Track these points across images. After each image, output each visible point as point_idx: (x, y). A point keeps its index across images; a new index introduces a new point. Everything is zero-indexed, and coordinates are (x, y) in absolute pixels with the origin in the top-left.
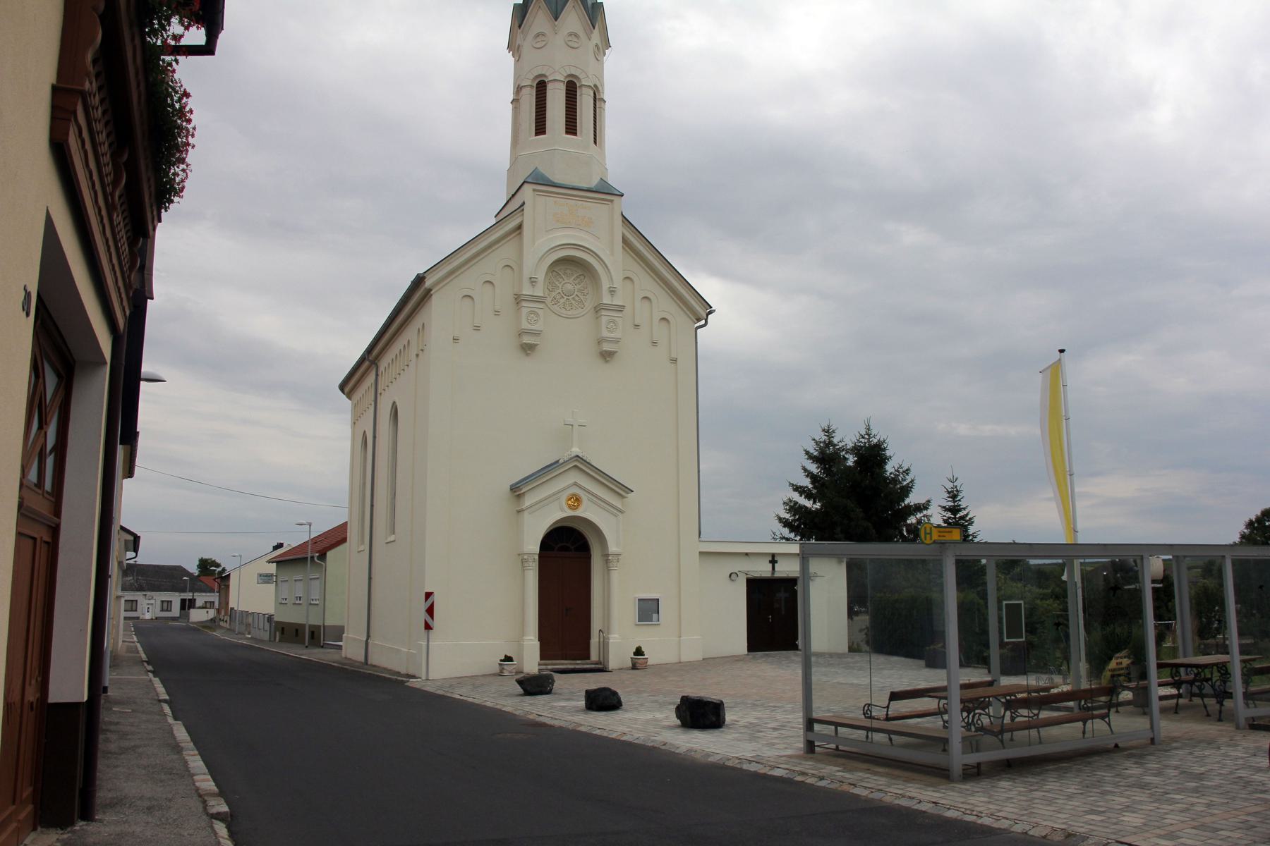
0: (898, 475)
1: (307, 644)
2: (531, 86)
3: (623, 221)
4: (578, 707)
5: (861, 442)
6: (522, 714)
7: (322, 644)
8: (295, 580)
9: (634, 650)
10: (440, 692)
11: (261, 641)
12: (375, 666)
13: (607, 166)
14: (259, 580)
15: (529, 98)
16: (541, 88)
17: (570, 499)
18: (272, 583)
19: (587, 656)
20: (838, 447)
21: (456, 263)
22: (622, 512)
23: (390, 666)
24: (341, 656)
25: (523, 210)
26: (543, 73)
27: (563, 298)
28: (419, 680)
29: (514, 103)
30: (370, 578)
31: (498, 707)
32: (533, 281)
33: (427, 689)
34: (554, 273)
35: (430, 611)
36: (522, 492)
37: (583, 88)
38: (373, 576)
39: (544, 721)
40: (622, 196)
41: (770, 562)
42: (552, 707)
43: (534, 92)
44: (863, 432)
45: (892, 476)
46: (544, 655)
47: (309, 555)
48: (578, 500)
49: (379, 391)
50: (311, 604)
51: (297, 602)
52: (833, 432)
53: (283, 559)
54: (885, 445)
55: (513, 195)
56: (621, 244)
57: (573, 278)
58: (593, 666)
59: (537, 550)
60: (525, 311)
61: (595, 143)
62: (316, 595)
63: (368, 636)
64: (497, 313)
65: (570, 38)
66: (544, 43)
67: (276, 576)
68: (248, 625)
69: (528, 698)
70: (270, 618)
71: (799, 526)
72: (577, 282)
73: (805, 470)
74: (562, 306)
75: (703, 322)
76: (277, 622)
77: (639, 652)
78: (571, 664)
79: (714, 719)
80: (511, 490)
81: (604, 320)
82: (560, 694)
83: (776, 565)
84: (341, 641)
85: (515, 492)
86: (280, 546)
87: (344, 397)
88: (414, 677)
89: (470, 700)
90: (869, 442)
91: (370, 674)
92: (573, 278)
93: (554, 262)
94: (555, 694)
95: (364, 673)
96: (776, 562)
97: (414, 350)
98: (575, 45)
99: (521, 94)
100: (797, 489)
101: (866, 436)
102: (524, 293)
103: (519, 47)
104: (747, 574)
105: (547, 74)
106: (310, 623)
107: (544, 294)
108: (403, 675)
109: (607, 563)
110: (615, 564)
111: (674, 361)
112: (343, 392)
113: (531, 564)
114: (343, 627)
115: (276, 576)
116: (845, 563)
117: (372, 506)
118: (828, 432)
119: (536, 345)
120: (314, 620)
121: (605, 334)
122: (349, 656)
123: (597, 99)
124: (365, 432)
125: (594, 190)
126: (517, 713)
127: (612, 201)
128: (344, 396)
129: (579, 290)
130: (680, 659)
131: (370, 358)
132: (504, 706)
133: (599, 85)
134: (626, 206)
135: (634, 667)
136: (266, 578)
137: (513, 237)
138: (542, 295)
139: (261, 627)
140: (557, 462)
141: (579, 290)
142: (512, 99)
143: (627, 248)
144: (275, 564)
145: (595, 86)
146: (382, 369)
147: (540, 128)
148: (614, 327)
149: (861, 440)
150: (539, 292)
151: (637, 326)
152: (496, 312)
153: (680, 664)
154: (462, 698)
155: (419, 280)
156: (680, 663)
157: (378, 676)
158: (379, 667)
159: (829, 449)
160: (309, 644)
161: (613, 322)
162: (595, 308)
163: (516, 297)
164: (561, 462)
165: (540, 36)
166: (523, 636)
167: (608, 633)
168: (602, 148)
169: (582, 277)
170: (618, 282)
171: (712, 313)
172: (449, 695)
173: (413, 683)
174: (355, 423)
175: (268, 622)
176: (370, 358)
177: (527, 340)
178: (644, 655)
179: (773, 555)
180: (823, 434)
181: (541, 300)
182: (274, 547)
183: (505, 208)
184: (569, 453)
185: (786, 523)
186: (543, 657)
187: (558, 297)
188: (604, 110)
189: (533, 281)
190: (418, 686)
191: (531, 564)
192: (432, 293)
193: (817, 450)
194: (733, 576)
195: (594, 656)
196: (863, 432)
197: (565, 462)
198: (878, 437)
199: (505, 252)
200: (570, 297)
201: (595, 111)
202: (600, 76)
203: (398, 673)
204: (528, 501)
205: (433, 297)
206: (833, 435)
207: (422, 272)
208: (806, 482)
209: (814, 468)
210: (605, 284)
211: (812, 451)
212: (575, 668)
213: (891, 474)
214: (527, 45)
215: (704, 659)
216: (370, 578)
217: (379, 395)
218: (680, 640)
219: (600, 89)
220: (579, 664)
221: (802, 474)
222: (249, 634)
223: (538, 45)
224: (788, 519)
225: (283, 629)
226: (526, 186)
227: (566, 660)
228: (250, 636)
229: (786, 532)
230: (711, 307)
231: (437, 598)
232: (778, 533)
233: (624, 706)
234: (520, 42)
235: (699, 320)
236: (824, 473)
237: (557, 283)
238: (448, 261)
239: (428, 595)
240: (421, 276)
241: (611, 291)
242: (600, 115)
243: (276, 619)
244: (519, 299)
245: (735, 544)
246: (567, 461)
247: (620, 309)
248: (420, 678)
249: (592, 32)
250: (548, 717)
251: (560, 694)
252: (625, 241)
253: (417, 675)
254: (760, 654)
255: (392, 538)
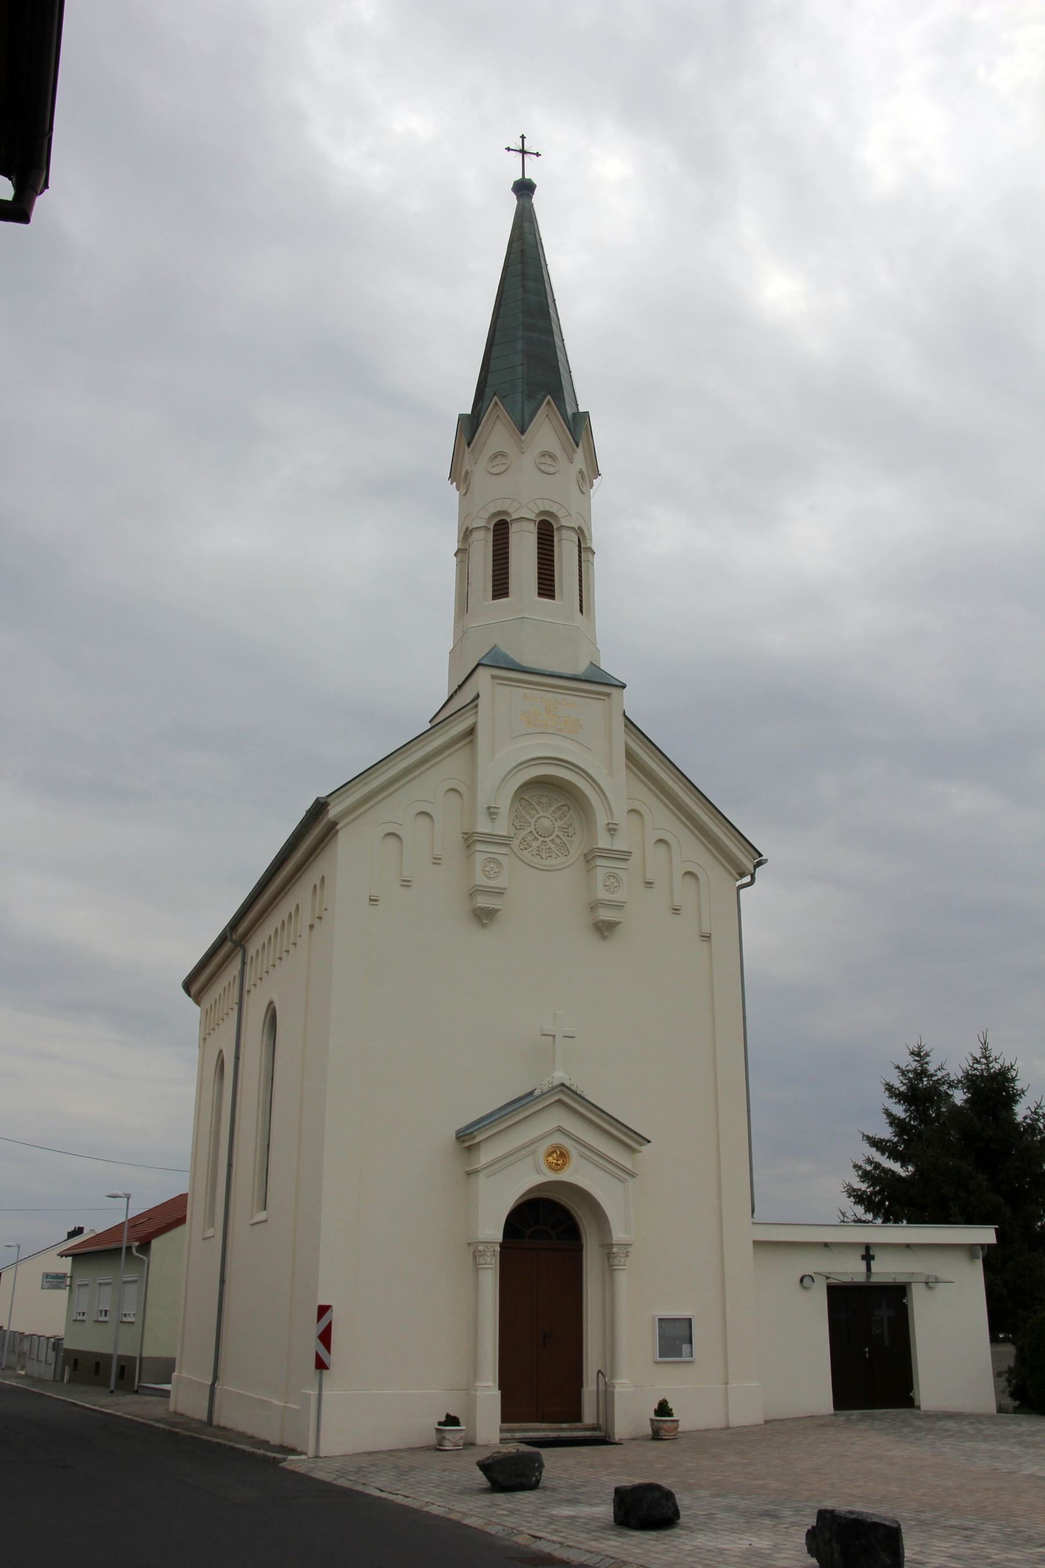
0: (1038, 1120)
1: (112, 1387)
2: (486, 528)
3: (626, 725)
4: (595, 1519)
5: (976, 1069)
6: (499, 1534)
7: (136, 1388)
8: (100, 1284)
9: (656, 1407)
10: (342, 1482)
11: (40, 1381)
12: (224, 1429)
13: (598, 646)
14: (45, 1283)
15: (483, 547)
16: (501, 531)
17: (550, 1154)
18: (65, 1289)
19: (576, 1416)
20: (935, 1078)
21: (374, 784)
22: (633, 1175)
23: (250, 1430)
24: (168, 1409)
25: (477, 706)
26: (504, 508)
27: (538, 839)
28: (303, 1457)
29: (459, 555)
30: (222, 1282)
31: (452, 1516)
32: (492, 813)
33: (318, 1475)
34: (523, 801)
35: (325, 1337)
36: (476, 1140)
37: (564, 531)
38: (227, 1278)
39: (547, 1550)
40: (624, 687)
41: (863, 1258)
42: (552, 1519)
43: (490, 536)
44: (978, 1055)
45: (1028, 1121)
46: (509, 1413)
47: (124, 1246)
48: (563, 1155)
49: (246, 988)
50: (122, 1322)
51: (100, 1319)
52: (927, 1055)
53: (90, 1249)
54: (1014, 1073)
55: (460, 687)
56: (624, 760)
57: (552, 809)
58: (588, 1434)
59: (498, 1235)
60: (479, 858)
61: (581, 611)
62: (131, 1310)
63: (215, 1378)
64: (437, 861)
65: (543, 460)
66: (504, 467)
67: (71, 1277)
68: (22, 1355)
69: (500, 1497)
70: (57, 1344)
71: (881, 1203)
72: (557, 815)
73: (889, 1114)
74: (535, 852)
75: (747, 879)
76: (67, 1351)
77: (663, 1409)
78: (551, 1430)
79: (888, 1561)
80: (458, 1138)
81: (600, 873)
82: (553, 1489)
83: (872, 1262)
84: (170, 1383)
85: (464, 1141)
86: (79, 1231)
87: (190, 1000)
88: (293, 1451)
89: (399, 1499)
90: (988, 1069)
91: (218, 1444)
92: (552, 809)
93: (519, 788)
94: (545, 1488)
95: (208, 1442)
96: (873, 1258)
97: (306, 918)
98: (551, 470)
99: (471, 540)
100: (877, 1144)
101: (983, 1060)
102: (479, 830)
103: (467, 473)
104: (827, 1278)
105: (510, 511)
106: (121, 1352)
107: (508, 832)
108: (273, 1446)
109: (609, 1258)
110: (622, 1260)
111: (706, 937)
112: (189, 994)
113: (489, 1259)
114: (174, 1359)
115: (71, 1277)
116: (981, 1258)
117: (230, 1165)
118: (918, 1054)
119: (497, 911)
120: (127, 1349)
121: (602, 894)
122: (180, 1410)
123: (584, 549)
124: (221, 1051)
125: (583, 678)
126: (492, 1530)
127: (608, 695)
128: (190, 1000)
129: (561, 828)
130: (728, 1421)
131: (234, 937)
132: (465, 1514)
133: (585, 529)
134: (632, 702)
135: (656, 1436)
136: (54, 1281)
137: (464, 746)
138: (505, 833)
139: (42, 1358)
140: (531, 1093)
141: (561, 828)
142: (456, 549)
143: (633, 768)
144: (70, 1259)
145: (580, 528)
146: (252, 952)
147: (501, 588)
148: (616, 884)
149: (975, 1066)
150: (502, 827)
151: (649, 884)
152: (435, 858)
153: (727, 1432)
154: (384, 1495)
155: (319, 808)
156: (728, 1428)
157: (232, 1448)
158: (231, 1430)
159: (923, 1081)
160: (117, 1387)
161: (614, 876)
162: (585, 855)
163: (466, 836)
164: (537, 1093)
165: (499, 457)
166: (475, 1380)
167: (613, 1376)
168: (591, 619)
169: (565, 809)
170: (620, 817)
171: (762, 864)
172: (359, 1488)
173: (293, 1462)
174: (205, 1039)
175: (54, 1349)
176: (234, 937)
177: (483, 902)
178: (671, 1415)
179: (868, 1247)
180: (911, 1059)
181: (503, 841)
182: (69, 1233)
183: (444, 710)
184: (550, 1079)
185: (860, 1198)
186: (506, 1417)
187: (530, 838)
188: (593, 565)
189: (492, 813)
190: (302, 1470)
191: (489, 1259)
192: (337, 827)
193: (904, 1084)
194: (806, 1281)
195: (589, 1416)
196: (978, 1055)
197: (543, 1094)
198: (1000, 1061)
199: (452, 767)
200: (548, 839)
201: (580, 566)
202: (586, 513)
203: (265, 1444)
204: (485, 1156)
205: (340, 834)
206: (928, 1059)
207: (324, 795)
208: (886, 1133)
209: (899, 1111)
210: (601, 819)
211: (897, 1084)
212: (559, 1437)
213: (1025, 1118)
214: (479, 471)
215: (766, 1422)
216: (222, 1282)
217: (245, 993)
218: (726, 1389)
219: (586, 533)
220: (565, 1430)
221: (884, 1120)
222: (22, 1368)
223: (496, 470)
224: (865, 1191)
225: (76, 1361)
226: (481, 671)
227: (543, 1421)
228: (23, 1373)
229: (860, 1210)
230: (760, 855)
231: (338, 1318)
232: (850, 1214)
233: (682, 1520)
234: (469, 468)
235: (742, 875)
236: (915, 1119)
237: (528, 817)
238: (364, 779)
239: (323, 1310)
240: (323, 801)
241: (610, 830)
242: (588, 572)
243: (67, 1345)
244: (470, 840)
245: (791, 1227)
246: (547, 1092)
247: (623, 856)
248: (305, 1454)
249: (574, 452)
250: (553, 1542)
251: (553, 1489)
252: (630, 755)
253: (299, 1449)
254: (855, 1414)
255: (262, 1216)
